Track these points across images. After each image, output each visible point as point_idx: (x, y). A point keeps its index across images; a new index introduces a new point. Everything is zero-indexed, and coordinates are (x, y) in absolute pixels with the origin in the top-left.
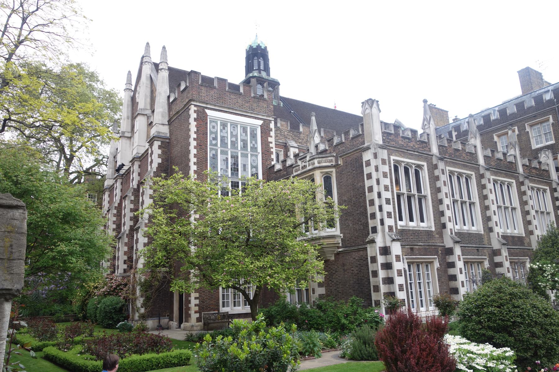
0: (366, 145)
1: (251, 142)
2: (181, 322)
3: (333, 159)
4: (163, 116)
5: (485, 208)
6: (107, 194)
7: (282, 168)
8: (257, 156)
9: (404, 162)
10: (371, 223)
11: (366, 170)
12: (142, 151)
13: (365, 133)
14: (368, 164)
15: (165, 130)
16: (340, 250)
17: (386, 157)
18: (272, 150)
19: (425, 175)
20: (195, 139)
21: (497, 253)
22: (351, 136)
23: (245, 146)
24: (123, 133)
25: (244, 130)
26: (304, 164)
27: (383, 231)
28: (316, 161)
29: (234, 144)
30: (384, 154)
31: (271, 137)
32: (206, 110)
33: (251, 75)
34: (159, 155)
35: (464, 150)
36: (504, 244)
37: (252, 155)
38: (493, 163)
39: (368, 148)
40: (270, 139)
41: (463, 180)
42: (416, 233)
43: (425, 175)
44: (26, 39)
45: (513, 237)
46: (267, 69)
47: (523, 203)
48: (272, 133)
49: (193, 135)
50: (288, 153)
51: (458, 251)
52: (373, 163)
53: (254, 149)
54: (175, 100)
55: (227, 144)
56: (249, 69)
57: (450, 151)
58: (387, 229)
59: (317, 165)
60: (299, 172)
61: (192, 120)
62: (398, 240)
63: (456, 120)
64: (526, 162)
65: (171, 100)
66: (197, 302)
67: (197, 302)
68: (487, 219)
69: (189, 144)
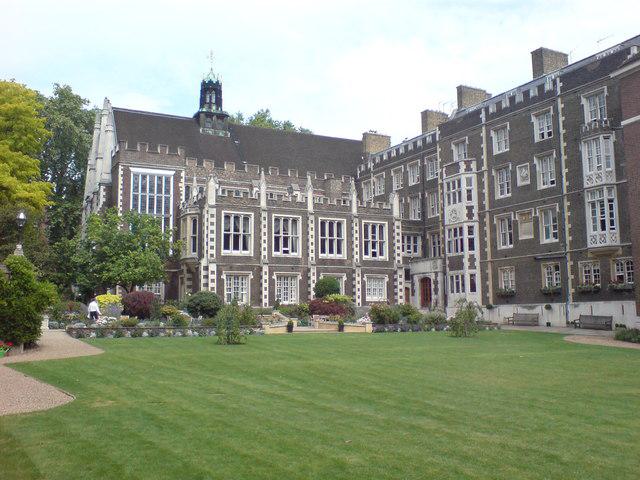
19: (252, 221)
25: (160, 178)
40: (180, 185)
41: (335, 226)
43: (252, 221)
46: (219, 102)
48: (183, 180)
51: (358, 271)
56: (203, 102)
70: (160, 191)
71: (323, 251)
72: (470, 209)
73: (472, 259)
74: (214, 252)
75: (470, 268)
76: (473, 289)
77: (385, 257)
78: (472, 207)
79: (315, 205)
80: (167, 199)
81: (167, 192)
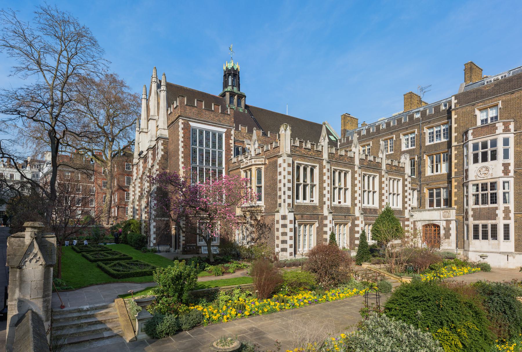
1: (218, 143)
2: (176, 249)
3: (263, 159)
4: (164, 124)
5: (354, 192)
6: (135, 167)
10: (279, 201)
11: (279, 170)
12: (154, 143)
13: (281, 146)
15: (166, 133)
17: (291, 162)
19: (316, 171)
20: (182, 142)
21: (357, 219)
22: (273, 147)
24: (143, 129)
25: (214, 135)
27: (284, 206)
28: (253, 160)
30: (290, 160)
32: (190, 122)
33: (226, 90)
34: (162, 149)
35: (346, 155)
36: (361, 214)
38: (365, 164)
39: (281, 156)
42: (306, 207)
44: (70, 75)
45: (370, 209)
47: (381, 188)
48: (232, 138)
49: (181, 139)
51: (330, 217)
52: (286, 181)
54: (171, 113)
56: (225, 85)
57: (336, 156)
58: (287, 205)
59: (253, 163)
60: (244, 166)
61: (180, 129)
62: (292, 212)
63: (364, 124)
64: (389, 162)
65: (169, 112)
66: (184, 238)
67: (184, 238)
68: (353, 198)
69: (179, 145)
70: (214, 146)
71: (298, 198)
72: (506, 166)
73: (507, 211)
74: (290, 201)
75: (504, 218)
76: (507, 237)
77: (348, 203)
78: (509, 164)
79: (330, 155)
80: (220, 154)
81: (220, 147)
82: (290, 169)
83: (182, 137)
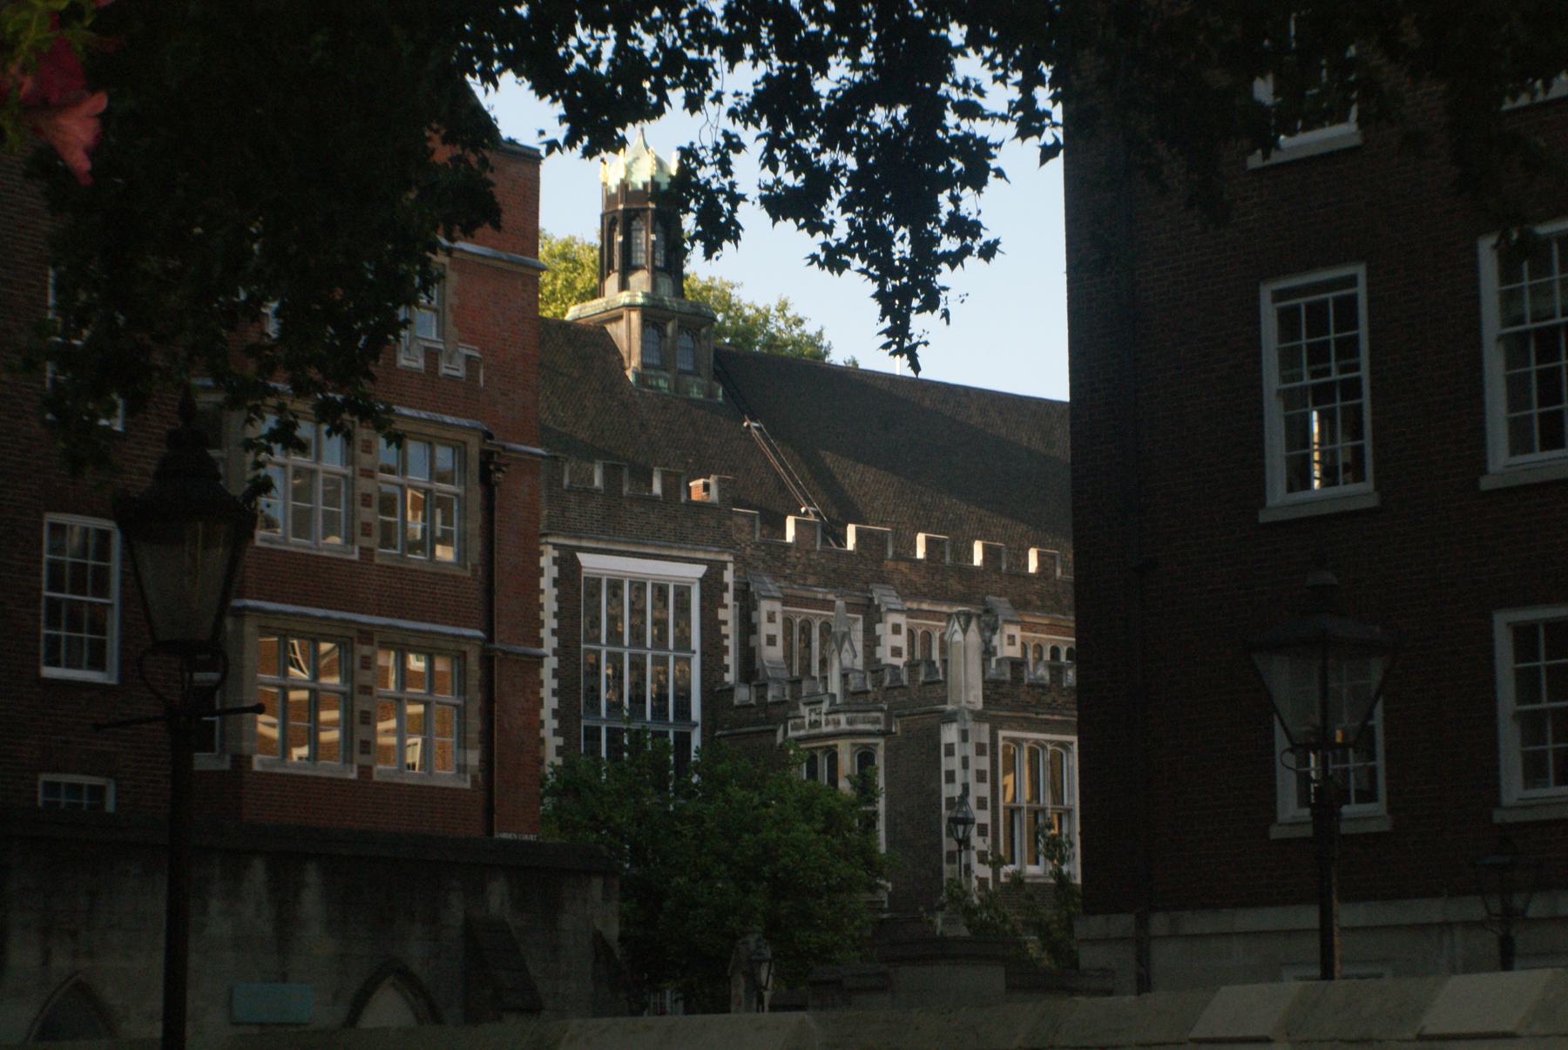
0: (949, 707)
1: (676, 625)
7: (753, 701)
8: (688, 661)
9: (1026, 740)
11: (947, 764)
14: (950, 751)
16: (885, 916)
17: (986, 740)
18: (726, 642)
22: (922, 678)
23: (660, 640)
26: (814, 717)
29: (638, 636)
30: (983, 733)
31: (726, 606)
34: (558, 748)
37: (677, 659)
40: (722, 614)
48: (728, 598)
50: (754, 614)
53: (683, 642)
55: (621, 634)
59: (844, 726)
60: (802, 733)
61: (545, 583)
82: (985, 763)
83: (556, 615)
